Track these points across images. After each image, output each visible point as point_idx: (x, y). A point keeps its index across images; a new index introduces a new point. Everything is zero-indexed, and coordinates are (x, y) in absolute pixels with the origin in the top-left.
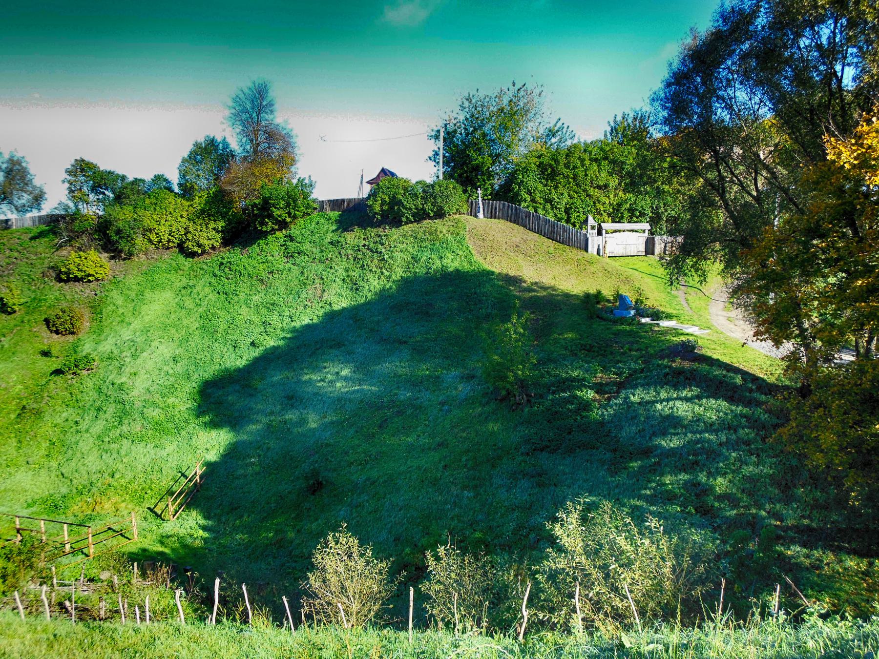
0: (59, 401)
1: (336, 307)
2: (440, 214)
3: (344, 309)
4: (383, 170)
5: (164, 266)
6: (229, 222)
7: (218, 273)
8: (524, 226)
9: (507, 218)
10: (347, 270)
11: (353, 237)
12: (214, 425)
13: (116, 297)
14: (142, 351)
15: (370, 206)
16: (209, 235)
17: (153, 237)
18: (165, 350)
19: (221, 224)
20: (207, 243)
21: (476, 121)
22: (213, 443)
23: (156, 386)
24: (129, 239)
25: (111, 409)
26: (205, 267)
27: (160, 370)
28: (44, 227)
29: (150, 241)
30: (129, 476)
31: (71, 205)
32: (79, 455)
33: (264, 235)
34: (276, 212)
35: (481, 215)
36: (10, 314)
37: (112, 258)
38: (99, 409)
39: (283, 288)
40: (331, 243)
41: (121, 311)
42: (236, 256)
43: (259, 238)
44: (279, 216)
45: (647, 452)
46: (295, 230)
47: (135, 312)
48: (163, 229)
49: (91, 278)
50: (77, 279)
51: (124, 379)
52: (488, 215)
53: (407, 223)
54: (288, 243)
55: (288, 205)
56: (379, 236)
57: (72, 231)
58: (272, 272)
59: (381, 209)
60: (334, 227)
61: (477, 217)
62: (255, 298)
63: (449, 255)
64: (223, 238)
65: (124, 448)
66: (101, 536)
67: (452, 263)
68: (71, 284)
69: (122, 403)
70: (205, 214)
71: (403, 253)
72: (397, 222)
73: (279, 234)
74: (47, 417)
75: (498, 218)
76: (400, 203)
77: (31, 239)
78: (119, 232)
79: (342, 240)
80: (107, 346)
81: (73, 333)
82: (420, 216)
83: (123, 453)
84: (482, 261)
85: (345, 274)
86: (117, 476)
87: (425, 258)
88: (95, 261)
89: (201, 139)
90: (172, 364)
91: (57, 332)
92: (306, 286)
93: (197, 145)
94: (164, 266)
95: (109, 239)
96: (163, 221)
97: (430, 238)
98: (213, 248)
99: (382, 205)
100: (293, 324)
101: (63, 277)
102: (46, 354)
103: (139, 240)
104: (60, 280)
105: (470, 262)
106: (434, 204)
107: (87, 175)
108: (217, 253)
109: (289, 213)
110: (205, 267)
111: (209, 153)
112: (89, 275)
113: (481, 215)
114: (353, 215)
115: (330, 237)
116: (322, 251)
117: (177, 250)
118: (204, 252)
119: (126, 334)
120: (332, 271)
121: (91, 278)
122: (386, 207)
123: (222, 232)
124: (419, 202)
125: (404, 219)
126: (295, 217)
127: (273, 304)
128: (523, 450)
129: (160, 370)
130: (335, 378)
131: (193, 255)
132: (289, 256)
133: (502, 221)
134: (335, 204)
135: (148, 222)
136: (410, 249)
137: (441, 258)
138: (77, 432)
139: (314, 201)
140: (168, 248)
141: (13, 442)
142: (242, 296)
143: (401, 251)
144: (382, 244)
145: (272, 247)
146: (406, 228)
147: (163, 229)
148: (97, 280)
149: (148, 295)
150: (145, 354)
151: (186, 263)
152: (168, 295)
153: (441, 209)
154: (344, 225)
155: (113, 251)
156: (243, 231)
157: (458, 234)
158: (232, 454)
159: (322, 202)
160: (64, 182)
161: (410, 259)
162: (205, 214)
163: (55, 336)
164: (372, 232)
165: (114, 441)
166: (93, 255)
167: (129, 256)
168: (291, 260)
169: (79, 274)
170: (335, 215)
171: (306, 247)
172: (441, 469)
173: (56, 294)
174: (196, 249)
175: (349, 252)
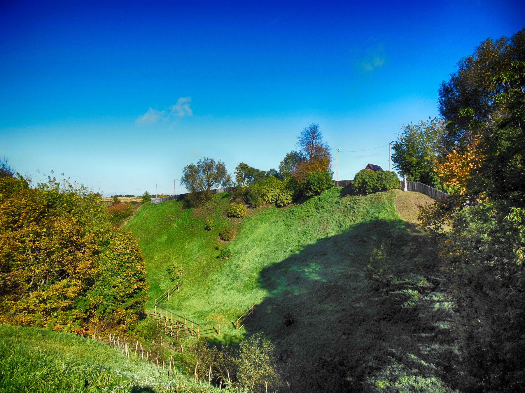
0: (216, 270)
1: (330, 235)
2: (384, 189)
3: (333, 236)
4: (368, 165)
5: (268, 211)
6: (296, 191)
7: (288, 215)
8: (429, 196)
9: (419, 191)
10: (339, 217)
11: (346, 200)
12: (263, 287)
13: (247, 225)
14: (250, 250)
15: (353, 184)
16: (287, 198)
17: (266, 198)
18: (258, 251)
19: (292, 192)
20: (286, 201)
21: (409, 140)
22: (259, 296)
23: (250, 267)
24: (256, 200)
25: (232, 275)
26: (284, 212)
27: (254, 260)
28: (227, 193)
29: (265, 200)
30: (230, 306)
31: (237, 183)
32: (216, 295)
33: (309, 198)
34: (313, 187)
35: (406, 189)
36: (209, 230)
37: (249, 207)
38: (228, 275)
39: (311, 224)
40: (336, 203)
41: (247, 231)
42: (298, 209)
43: (307, 199)
44: (315, 189)
45: (432, 329)
46: (322, 196)
47: (252, 233)
48: (270, 194)
49: (239, 216)
50: (234, 216)
51: (239, 263)
52: (411, 189)
53: (369, 193)
54: (318, 202)
55: (319, 183)
56: (356, 200)
57: (236, 195)
58: (308, 216)
59: (370, 183)
60: (339, 195)
61: (403, 190)
62: (299, 229)
63: (384, 211)
64: (293, 199)
65: (232, 294)
66: (210, 331)
67: (383, 215)
68: (232, 218)
69: (236, 273)
70: (287, 188)
71: (364, 209)
72: (364, 194)
73: (316, 198)
74: (210, 276)
75: (416, 191)
76: (366, 183)
77: (223, 198)
78: (251, 196)
79: (340, 201)
80: (237, 248)
81: (228, 240)
82: (375, 190)
83: (231, 296)
84: (399, 215)
85: (338, 218)
86: (226, 306)
87: (372, 212)
88: (241, 208)
89: (289, 153)
90: (258, 258)
91: (223, 239)
92: (325, 222)
93: (287, 155)
94: (268, 211)
95: (248, 198)
96: (270, 191)
97: (377, 201)
98: (288, 203)
99: (358, 184)
100: (310, 242)
101: (230, 216)
102: (217, 249)
103: (260, 199)
104: (229, 217)
105: (393, 215)
106: (381, 184)
107: (245, 170)
108: (290, 206)
109: (320, 188)
110: (284, 212)
111: (293, 158)
112: (239, 215)
113: (406, 189)
114: (348, 189)
115: (336, 199)
116: (331, 207)
117: (275, 204)
118: (284, 206)
119: (246, 242)
120: (332, 217)
121: (239, 216)
122: (360, 185)
123: (293, 196)
124: (375, 183)
125: (367, 191)
126: (323, 189)
127: (305, 232)
128: (375, 318)
129: (254, 260)
130: (313, 272)
131: (280, 207)
132: (317, 209)
133: (417, 193)
134: (342, 183)
135: (264, 191)
136: (367, 207)
137: (379, 212)
138: (218, 284)
139: (333, 181)
140: (271, 203)
141: (197, 286)
142: (294, 227)
143: (363, 208)
144: (356, 204)
145: (310, 205)
146: (368, 196)
147: (270, 194)
148: (241, 217)
149: (259, 225)
150: (250, 252)
151: (277, 210)
152: (267, 225)
153: (385, 186)
154: (343, 194)
155: (250, 204)
156: (300, 197)
157: (391, 200)
158: (267, 301)
159: (336, 182)
160: (234, 173)
161: (366, 212)
162: (287, 188)
163: (222, 241)
164: (354, 197)
165: (229, 290)
166: (241, 206)
167: (255, 207)
168: (318, 211)
169: (235, 214)
170: (340, 188)
171: (325, 204)
172: (337, 322)
173: (226, 222)
174: (281, 204)
175: (342, 207)
